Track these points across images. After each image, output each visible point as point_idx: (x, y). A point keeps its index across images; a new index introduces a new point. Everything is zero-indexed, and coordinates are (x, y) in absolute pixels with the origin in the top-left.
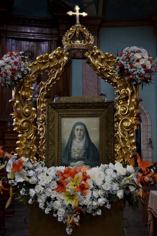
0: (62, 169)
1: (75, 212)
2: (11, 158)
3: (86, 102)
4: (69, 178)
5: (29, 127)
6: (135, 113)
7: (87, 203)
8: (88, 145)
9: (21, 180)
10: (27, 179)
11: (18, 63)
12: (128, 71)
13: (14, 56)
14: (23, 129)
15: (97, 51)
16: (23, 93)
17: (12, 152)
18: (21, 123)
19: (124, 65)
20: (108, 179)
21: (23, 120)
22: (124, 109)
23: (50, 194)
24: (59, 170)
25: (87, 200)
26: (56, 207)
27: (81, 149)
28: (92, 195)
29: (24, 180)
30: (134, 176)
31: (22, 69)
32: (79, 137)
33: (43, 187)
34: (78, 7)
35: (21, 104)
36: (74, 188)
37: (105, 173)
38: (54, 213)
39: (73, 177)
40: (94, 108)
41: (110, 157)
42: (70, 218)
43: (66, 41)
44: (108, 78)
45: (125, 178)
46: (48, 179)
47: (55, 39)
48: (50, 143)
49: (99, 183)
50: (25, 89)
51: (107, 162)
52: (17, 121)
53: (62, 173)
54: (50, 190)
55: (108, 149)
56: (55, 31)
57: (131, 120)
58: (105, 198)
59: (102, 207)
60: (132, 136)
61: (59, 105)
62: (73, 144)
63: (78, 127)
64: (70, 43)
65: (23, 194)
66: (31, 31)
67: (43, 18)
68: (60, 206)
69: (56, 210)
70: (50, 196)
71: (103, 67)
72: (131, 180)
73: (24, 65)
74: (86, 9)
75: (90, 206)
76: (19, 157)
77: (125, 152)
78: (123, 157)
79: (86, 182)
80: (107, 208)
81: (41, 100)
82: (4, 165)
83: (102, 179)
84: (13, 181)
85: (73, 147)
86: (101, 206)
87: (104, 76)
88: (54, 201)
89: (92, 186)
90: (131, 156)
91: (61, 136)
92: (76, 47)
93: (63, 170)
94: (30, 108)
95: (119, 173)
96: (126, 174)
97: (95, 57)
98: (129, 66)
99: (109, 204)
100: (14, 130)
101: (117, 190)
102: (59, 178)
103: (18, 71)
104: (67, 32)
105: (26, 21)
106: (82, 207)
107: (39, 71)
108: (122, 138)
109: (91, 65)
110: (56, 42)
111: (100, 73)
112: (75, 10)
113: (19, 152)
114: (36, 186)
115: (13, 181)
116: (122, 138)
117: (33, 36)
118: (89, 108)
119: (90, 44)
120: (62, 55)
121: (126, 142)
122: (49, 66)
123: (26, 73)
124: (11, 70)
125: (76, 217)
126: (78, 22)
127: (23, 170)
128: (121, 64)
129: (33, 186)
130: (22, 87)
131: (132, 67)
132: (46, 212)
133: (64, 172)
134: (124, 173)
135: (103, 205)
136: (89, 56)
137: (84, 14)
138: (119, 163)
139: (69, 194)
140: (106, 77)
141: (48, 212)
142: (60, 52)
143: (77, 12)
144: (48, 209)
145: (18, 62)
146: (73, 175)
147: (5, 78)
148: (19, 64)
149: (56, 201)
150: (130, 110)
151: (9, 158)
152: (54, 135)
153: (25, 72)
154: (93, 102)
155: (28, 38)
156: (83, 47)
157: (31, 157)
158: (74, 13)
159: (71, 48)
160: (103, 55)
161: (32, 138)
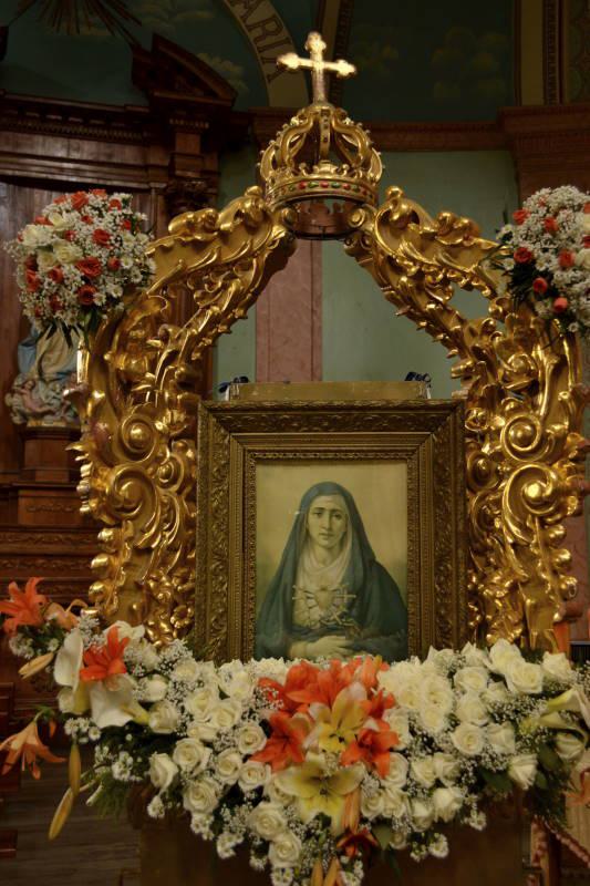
0: (276, 668)
1: (344, 847)
2: (73, 627)
3: (357, 403)
4: (315, 709)
5: (142, 499)
6: (572, 444)
7: (393, 810)
8: (360, 574)
9: (118, 719)
10: (142, 715)
11: (108, 235)
12: (549, 281)
13: (94, 208)
14: (119, 506)
15: (404, 207)
16: (121, 363)
17: (76, 602)
18: (112, 483)
19: (536, 255)
20: (471, 710)
21: (119, 473)
22: (523, 430)
23: (236, 775)
24: (267, 674)
25: (392, 796)
26: (264, 831)
27: (335, 590)
28: (408, 776)
29: (129, 718)
30: (581, 696)
31: (127, 263)
32: (326, 543)
33: (208, 744)
34: (319, 37)
35: (113, 407)
36: (335, 745)
37: (453, 687)
38: (252, 852)
39: (329, 703)
40: (385, 429)
41: (452, 619)
42: (324, 876)
43: (275, 164)
44: (431, 318)
45: (542, 706)
46: (225, 710)
47: (158, 185)
48: (213, 566)
49: (434, 725)
50: (130, 344)
51: (439, 640)
52: (94, 474)
53: (280, 685)
54: (236, 759)
55: (442, 588)
56: (157, 158)
57: (555, 471)
58: (461, 787)
59: (448, 826)
60: (557, 537)
61: (249, 416)
62: (304, 570)
63: (323, 502)
64: (296, 174)
65: (126, 777)
66: (68, 153)
67: (99, 104)
68: (280, 825)
69: (262, 839)
70: (237, 784)
71: (429, 266)
72: (567, 712)
73: (132, 245)
74: (269, 81)
75: (403, 819)
76: (103, 622)
77: (528, 601)
78: (524, 620)
79: (384, 722)
80: (474, 829)
81: (162, 396)
82: (48, 657)
83: (445, 708)
84: (82, 725)
85: (302, 582)
86: (446, 820)
87: (415, 306)
88: (255, 803)
89: (406, 739)
90: (556, 616)
91: (254, 537)
92: (319, 189)
93: (281, 674)
94: (147, 424)
95: (514, 685)
96: (544, 687)
97: (395, 228)
98: (555, 261)
99: (478, 812)
100: (84, 509)
101: (510, 755)
102: (272, 706)
103: (109, 270)
104: (282, 130)
105: (53, 117)
106: (372, 824)
107: (182, 278)
108: (514, 545)
109: (369, 263)
110: (160, 198)
111: (402, 296)
112: (310, 49)
113: (102, 602)
114: (178, 742)
115: (82, 722)
116: (514, 545)
117: (76, 172)
118: (368, 426)
119: (372, 181)
120: (266, 218)
121: (534, 558)
122: (219, 257)
123: (138, 280)
124: (79, 264)
125: (348, 868)
126: (320, 93)
127: (126, 676)
128: (523, 252)
129: (167, 743)
130: (117, 337)
131: (566, 263)
132: (220, 849)
133: (287, 681)
134: (533, 685)
135: (451, 817)
136: (373, 227)
137: (344, 68)
138: (505, 642)
139: (315, 774)
140: (420, 311)
141: (232, 853)
142: (257, 207)
143: (316, 58)
144: (230, 840)
145: (111, 231)
146: (328, 692)
147: (51, 297)
148: (116, 240)
149: (262, 805)
150: (549, 434)
151: (67, 627)
152: (227, 534)
153: (136, 276)
154: (384, 403)
155: (58, 177)
156: (345, 188)
157: (151, 623)
158: (306, 63)
159: (302, 191)
160: (427, 221)
161: (153, 546)
